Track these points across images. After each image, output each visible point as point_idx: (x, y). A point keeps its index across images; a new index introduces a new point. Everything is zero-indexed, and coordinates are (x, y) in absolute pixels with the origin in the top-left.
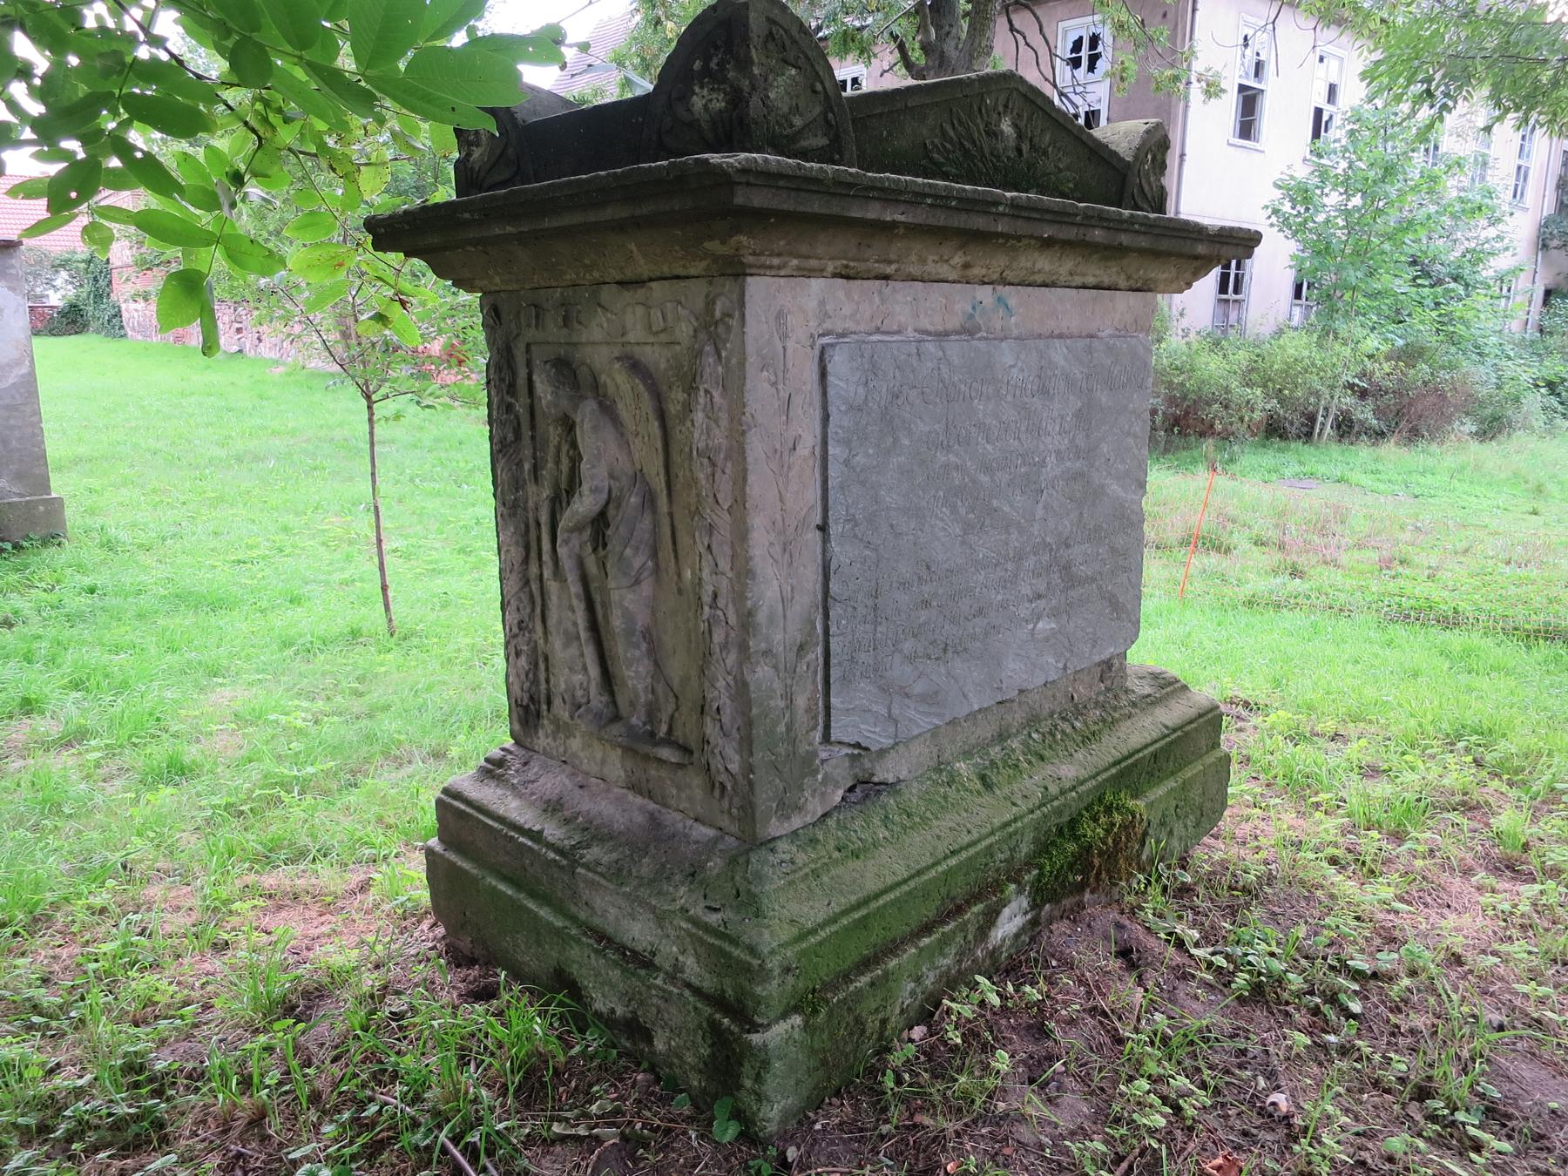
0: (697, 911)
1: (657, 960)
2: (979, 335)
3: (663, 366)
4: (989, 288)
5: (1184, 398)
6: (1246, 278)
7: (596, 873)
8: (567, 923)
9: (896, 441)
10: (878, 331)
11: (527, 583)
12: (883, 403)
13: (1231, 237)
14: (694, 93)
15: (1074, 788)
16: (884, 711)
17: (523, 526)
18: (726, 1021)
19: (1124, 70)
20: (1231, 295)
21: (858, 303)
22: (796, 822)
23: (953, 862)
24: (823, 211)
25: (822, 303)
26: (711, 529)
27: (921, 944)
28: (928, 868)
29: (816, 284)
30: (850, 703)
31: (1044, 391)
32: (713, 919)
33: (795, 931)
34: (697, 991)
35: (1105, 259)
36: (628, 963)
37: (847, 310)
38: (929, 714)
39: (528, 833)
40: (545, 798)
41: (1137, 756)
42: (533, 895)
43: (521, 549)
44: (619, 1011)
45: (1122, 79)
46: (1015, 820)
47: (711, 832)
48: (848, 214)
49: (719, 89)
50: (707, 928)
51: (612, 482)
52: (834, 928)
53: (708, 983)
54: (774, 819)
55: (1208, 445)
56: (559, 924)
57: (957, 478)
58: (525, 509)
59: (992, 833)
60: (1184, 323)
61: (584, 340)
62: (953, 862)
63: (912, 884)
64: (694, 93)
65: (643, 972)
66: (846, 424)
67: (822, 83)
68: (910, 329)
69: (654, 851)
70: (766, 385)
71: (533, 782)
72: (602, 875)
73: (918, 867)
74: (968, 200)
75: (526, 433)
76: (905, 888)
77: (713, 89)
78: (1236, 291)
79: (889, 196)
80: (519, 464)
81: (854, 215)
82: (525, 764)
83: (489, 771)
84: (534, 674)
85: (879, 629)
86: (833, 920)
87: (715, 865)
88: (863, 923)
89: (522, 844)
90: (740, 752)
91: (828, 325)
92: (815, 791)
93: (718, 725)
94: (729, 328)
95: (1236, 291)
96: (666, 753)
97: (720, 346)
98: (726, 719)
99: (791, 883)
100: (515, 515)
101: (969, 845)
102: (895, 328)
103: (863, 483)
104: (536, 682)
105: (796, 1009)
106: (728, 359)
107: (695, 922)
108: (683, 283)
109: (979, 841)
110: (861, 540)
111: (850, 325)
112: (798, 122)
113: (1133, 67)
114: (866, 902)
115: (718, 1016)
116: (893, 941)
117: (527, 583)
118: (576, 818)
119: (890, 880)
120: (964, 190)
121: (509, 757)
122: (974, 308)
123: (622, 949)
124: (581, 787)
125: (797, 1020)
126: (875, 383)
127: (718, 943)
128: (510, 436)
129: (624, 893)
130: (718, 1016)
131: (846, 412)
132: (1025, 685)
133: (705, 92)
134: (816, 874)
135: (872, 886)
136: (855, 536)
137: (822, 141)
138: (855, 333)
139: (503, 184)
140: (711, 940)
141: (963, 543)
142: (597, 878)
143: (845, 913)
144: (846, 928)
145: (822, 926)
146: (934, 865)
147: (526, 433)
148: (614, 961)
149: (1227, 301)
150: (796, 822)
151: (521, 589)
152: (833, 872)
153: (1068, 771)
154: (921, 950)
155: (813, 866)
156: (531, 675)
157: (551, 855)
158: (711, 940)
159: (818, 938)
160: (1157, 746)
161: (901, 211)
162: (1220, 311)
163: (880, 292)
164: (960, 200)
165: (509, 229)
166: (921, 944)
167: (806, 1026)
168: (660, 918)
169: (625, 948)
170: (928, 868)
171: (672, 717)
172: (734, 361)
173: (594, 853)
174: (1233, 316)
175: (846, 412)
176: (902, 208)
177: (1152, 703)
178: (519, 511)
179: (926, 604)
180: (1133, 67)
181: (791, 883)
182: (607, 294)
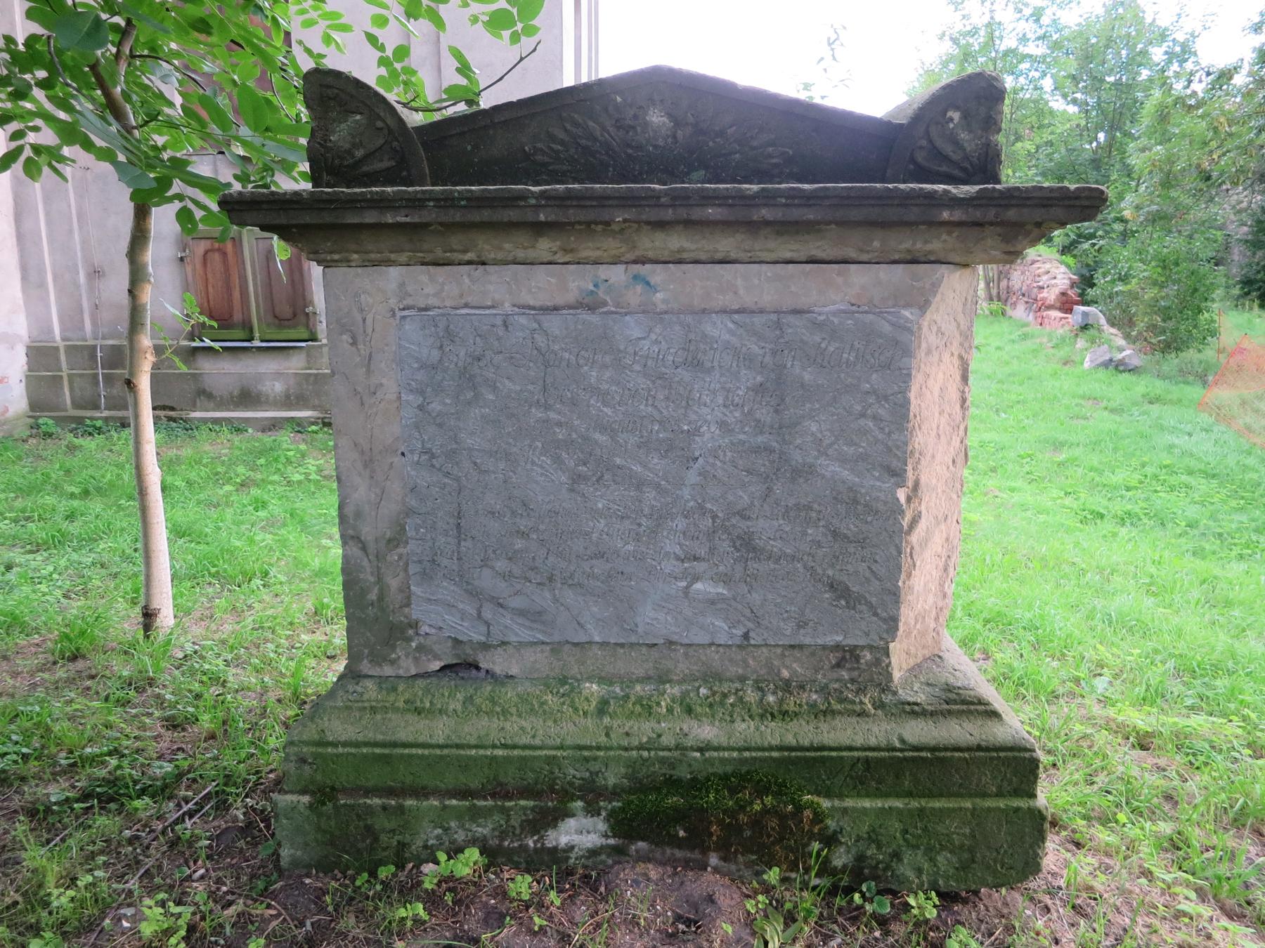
2: (605, 309)
4: (621, 268)
9: (477, 396)
10: (466, 306)
12: (460, 364)
13: (1013, 197)
15: (700, 750)
16: (474, 613)
21: (443, 284)
22: (388, 671)
23: (500, 752)
24: (314, 222)
25: (402, 285)
27: (447, 803)
28: (470, 747)
29: (394, 272)
30: (433, 595)
31: (696, 364)
33: (316, 737)
35: (779, 234)
37: (430, 289)
38: (531, 629)
41: (825, 753)
46: (599, 748)
48: (344, 222)
52: (353, 750)
54: (365, 661)
57: (561, 434)
59: (561, 747)
62: (500, 752)
63: (446, 751)
66: (419, 378)
67: (383, 121)
68: (507, 305)
70: (347, 346)
73: (458, 742)
74: (477, 199)
76: (438, 752)
79: (382, 203)
81: (349, 221)
85: (463, 543)
86: (357, 745)
88: (386, 759)
91: (409, 301)
92: (409, 654)
99: (348, 708)
101: (525, 747)
102: (489, 304)
103: (440, 425)
105: (313, 793)
109: (541, 748)
110: (439, 470)
111: (432, 301)
112: (359, 153)
114: (394, 745)
116: (424, 788)
119: (421, 739)
120: (471, 191)
122: (596, 286)
125: (306, 799)
126: (451, 347)
131: (419, 369)
132: (675, 638)
134: (373, 710)
135: (402, 736)
136: (433, 466)
137: (386, 164)
138: (439, 308)
141: (572, 490)
143: (366, 744)
144: (365, 756)
145: (345, 744)
146: (476, 747)
150: (388, 671)
152: (389, 716)
153: (706, 731)
154: (445, 807)
155: (374, 704)
159: (335, 751)
160: (875, 754)
161: (403, 214)
163: (469, 275)
164: (468, 199)
166: (447, 803)
167: (310, 806)
170: (470, 747)
175: (419, 369)
176: (403, 212)
177: (913, 713)
179: (524, 535)
181: (348, 708)
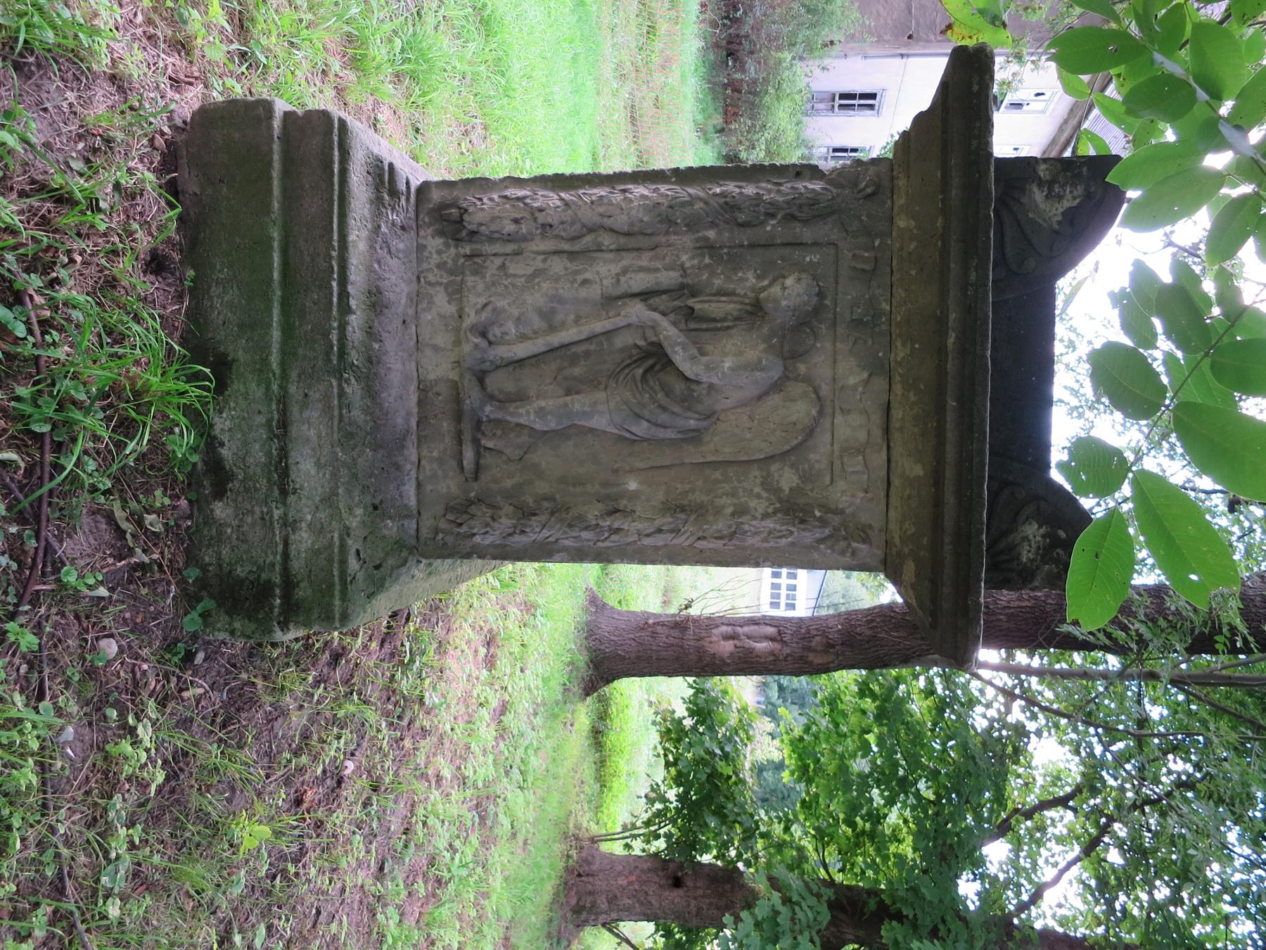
0: (353, 545)
1: (291, 499)
3: (812, 456)
5: (755, 94)
6: (852, 112)
7: (340, 408)
8: (278, 372)
11: (591, 230)
14: (1040, 526)
17: (649, 231)
18: (278, 601)
19: (1034, 10)
20: (838, 102)
26: (676, 531)
32: (353, 564)
34: (286, 556)
36: (276, 470)
39: (344, 295)
40: (381, 284)
42: (285, 304)
43: (626, 228)
44: (224, 452)
45: (1026, 9)
47: (413, 502)
49: (1037, 554)
50: (343, 562)
51: (705, 386)
53: (297, 565)
55: (718, 120)
56: (275, 366)
58: (667, 233)
60: (817, 72)
61: (839, 345)
64: (1040, 526)
65: (276, 492)
69: (379, 456)
71: (390, 252)
72: (341, 415)
75: (744, 237)
77: (1038, 548)
78: (841, 106)
80: (713, 225)
82: (403, 228)
83: (381, 176)
84: (498, 239)
87: (390, 528)
89: (331, 287)
90: (492, 545)
93: (511, 531)
94: (843, 553)
95: (841, 106)
96: (469, 455)
97: (829, 543)
98: (517, 538)
100: (661, 222)
104: (491, 239)
106: (817, 549)
107: (343, 546)
108: (882, 494)
113: (1034, 18)
115: (278, 591)
117: (591, 230)
118: (375, 341)
121: (403, 199)
123: (284, 453)
124: (404, 322)
127: (337, 579)
128: (742, 217)
129: (335, 453)
130: (278, 591)
133: (1038, 538)
139: (1000, 246)
140: (336, 573)
142: (336, 413)
147: (744, 237)
148: (271, 453)
149: (833, 100)
151: (584, 225)
156: (496, 235)
157: (334, 337)
158: (336, 573)
162: (824, 96)
165: (951, 340)
168: (329, 500)
169: (286, 457)
171: (500, 452)
172: (816, 556)
173: (354, 389)
174: (821, 106)
178: (665, 226)
180: (1034, 18)
182: (880, 383)
